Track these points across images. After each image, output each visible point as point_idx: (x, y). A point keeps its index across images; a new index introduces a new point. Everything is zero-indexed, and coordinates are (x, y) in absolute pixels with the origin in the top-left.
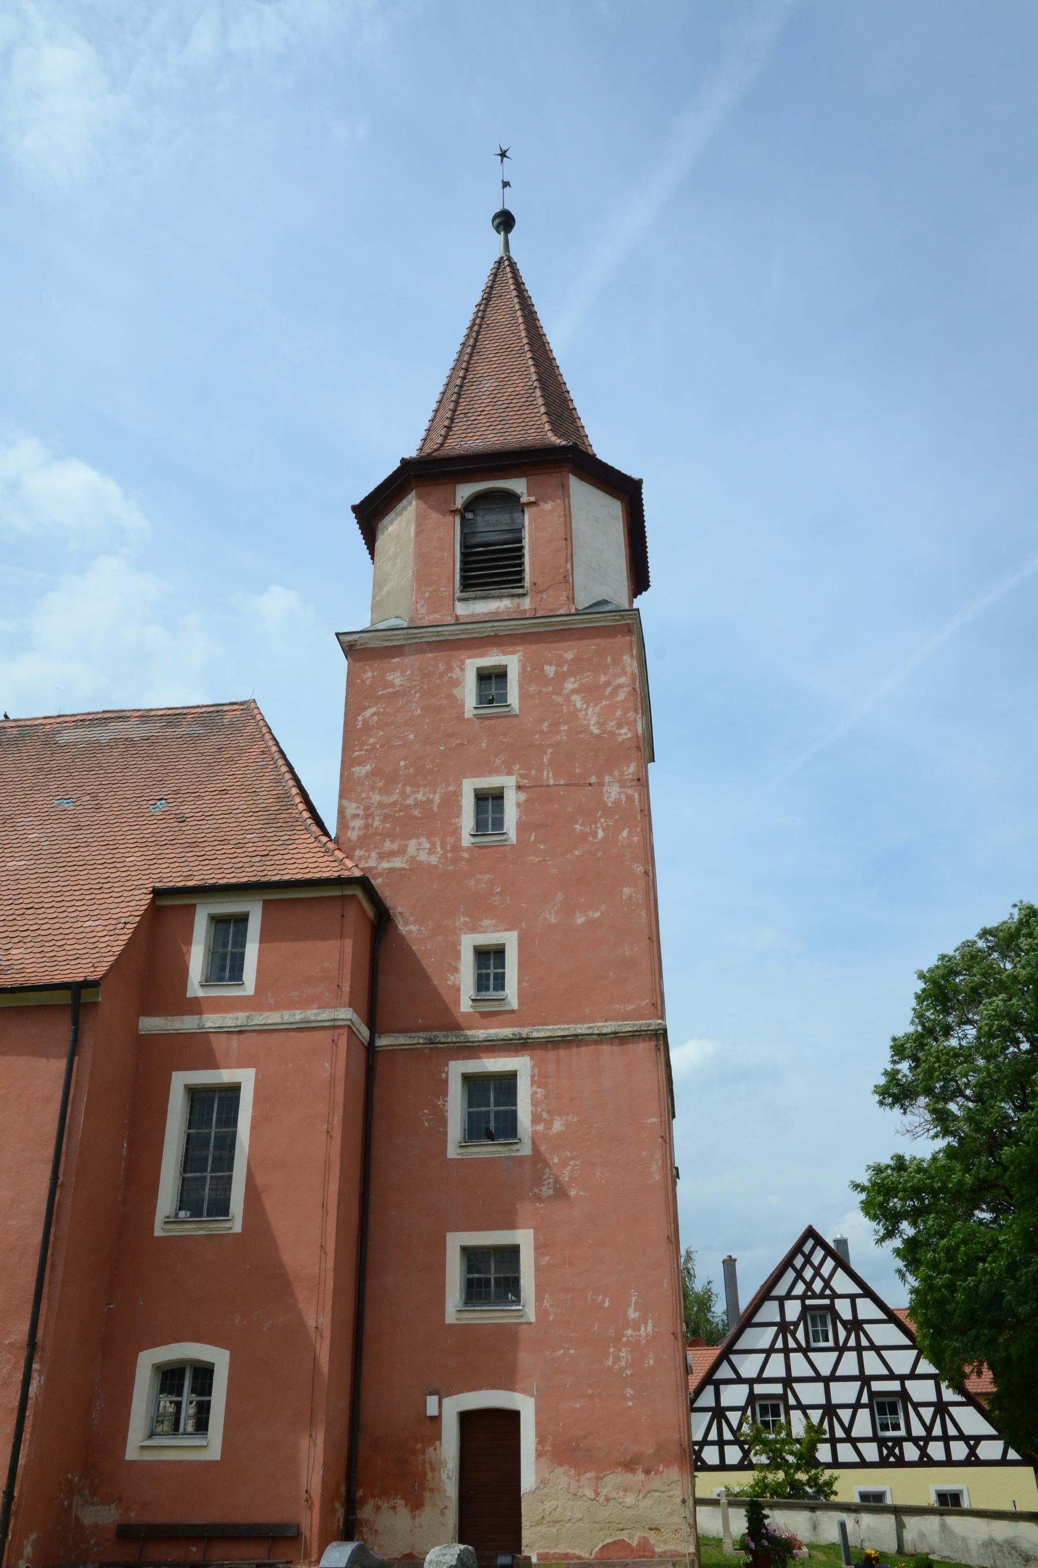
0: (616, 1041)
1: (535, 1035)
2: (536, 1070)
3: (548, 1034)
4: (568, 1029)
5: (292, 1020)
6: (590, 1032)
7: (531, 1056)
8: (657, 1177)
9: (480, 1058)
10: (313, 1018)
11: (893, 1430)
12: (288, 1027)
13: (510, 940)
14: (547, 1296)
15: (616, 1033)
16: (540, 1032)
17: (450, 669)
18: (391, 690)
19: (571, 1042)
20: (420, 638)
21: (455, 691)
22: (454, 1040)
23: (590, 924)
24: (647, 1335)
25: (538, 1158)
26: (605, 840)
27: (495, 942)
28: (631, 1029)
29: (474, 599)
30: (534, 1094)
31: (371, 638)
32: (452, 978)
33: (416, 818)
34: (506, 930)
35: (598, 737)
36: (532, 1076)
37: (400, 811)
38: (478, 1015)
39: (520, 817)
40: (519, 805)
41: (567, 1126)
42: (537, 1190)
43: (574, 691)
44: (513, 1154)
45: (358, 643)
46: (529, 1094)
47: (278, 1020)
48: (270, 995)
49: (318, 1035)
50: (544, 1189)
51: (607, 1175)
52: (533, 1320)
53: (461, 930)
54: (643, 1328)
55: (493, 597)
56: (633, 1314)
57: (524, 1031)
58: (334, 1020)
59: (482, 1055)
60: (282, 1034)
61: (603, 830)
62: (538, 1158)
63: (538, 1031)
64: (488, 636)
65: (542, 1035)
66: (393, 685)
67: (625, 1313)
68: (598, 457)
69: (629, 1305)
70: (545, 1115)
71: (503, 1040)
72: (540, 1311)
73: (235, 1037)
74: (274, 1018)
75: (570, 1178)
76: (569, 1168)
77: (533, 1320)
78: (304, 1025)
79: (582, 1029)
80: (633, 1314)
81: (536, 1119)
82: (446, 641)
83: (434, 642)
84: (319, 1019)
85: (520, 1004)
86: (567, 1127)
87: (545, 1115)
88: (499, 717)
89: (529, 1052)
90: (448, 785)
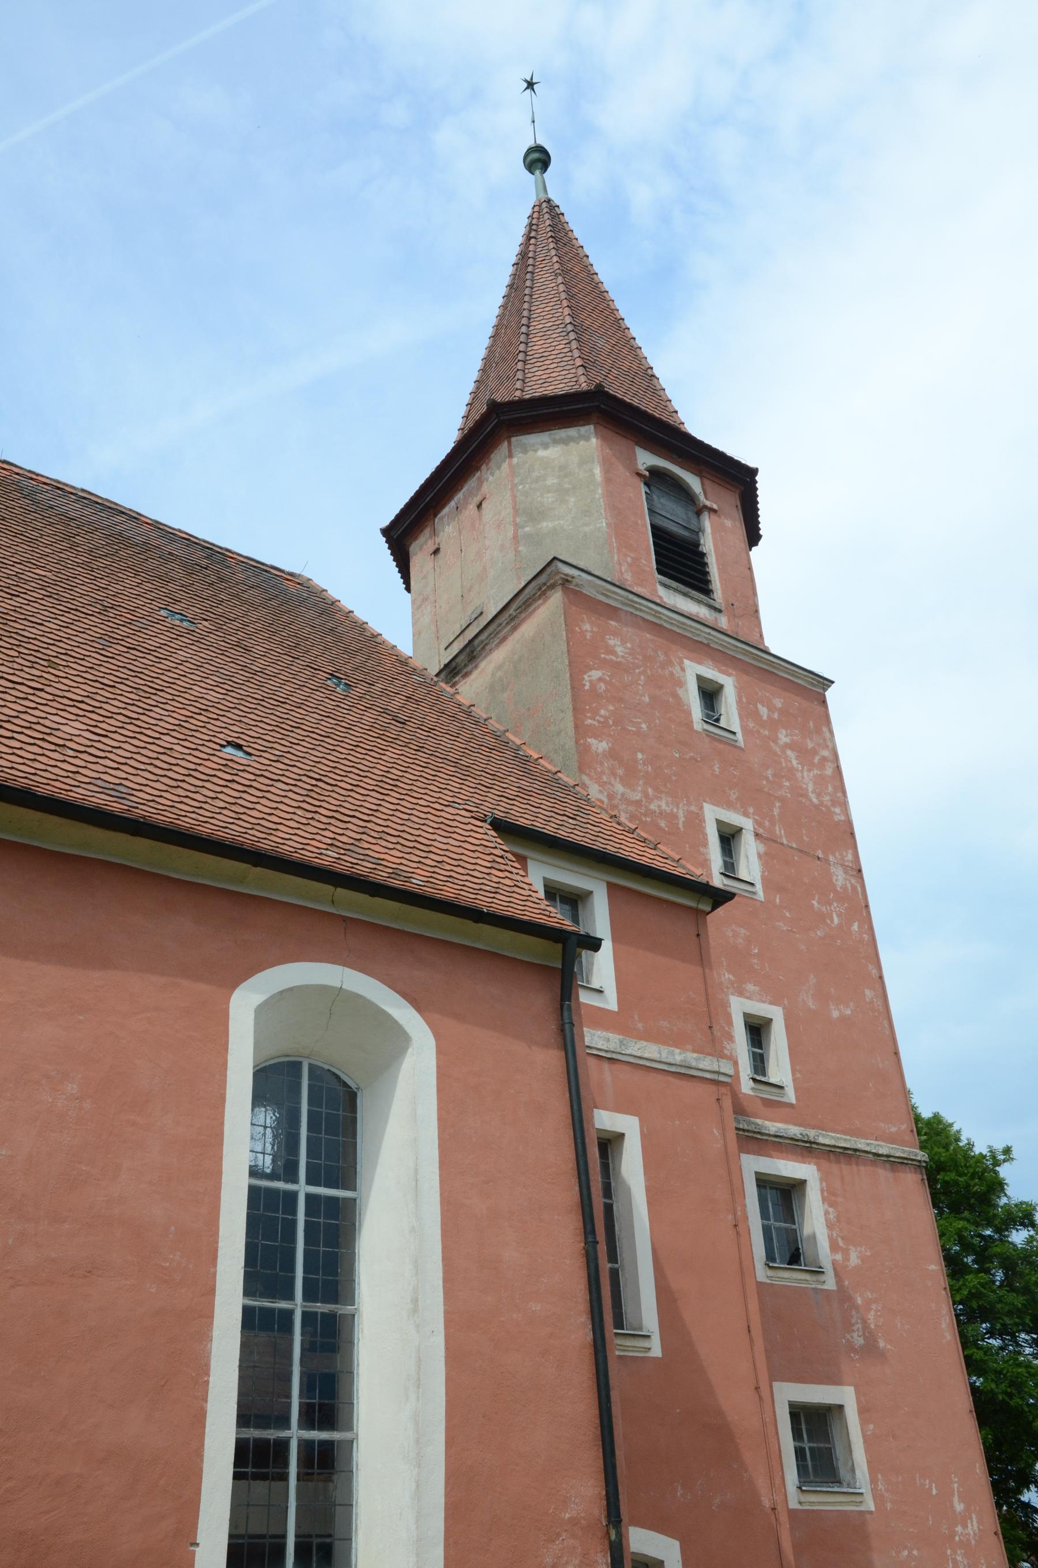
0: (888, 1166)
1: (821, 1140)
2: (824, 1184)
3: (832, 1142)
4: (850, 1140)
5: (670, 1060)
6: (868, 1149)
7: (816, 1164)
8: (949, 1338)
9: (771, 1156)
10: (694, 1064)
11: (243, 1452)
12: (666, 1067)
13: (775, 1014)
14: (880, 1476)
15: (888, 1156)
16: (826, 1139)
17: (670, 663)
18: (613, 657)
19: (850, 1156)
20: (637, 609)
21: (680, 692)
22: (746, 1127)
23: (843, 1018)
24: (975, 1534)
25: (843, 1295)
26: (840, 926)
27: (762, 1014)
28: (902, 1155)
29: (675, 590)
30: (826, 1213)
31: (589, 582)
32: (728, 1047)
33: (660, 829)
34: (771, 1003)
35: (817, 807)
36: (822, 1191)
37: (645, 815)
38: (759, 1102)
39: (763, 872)
40: (760, 856)
41: (863, 1259)
42: (848, 1336)
43: (787, 746)
44: (819, 1287)
45: (575, 581)
46: (823, 1213)
47: (655, 1056)
48: (636, 1017)
49: (699, 1089)
50: (855, 1335)
51: (907, 1327)
52: (873, 1509)
53: (727, 988)
54: (969, 1525)
55: (692, 598)
56: (959, 1507)
57: (812, 1134)
58: (718, 1073)
59: (773, 1153)
60: (660, 1077)
61: (838, 916)
62: (843, 1295)
63: (823, 1136)
64: (701, 642)
65: (827, 1141)
66: (614, 653)
67: (952, 1506)
68: (384, 539)
69: (953, 1495)
70: (841, 1243)
71: (792, 1139)
72: (877, 1497)
73: (606, 1065)
74: (650, 1050)
75: (876, 1325)
76: (872, 1313)
77: (873, 1509)
78: (683, 1071)
79: (861, 1144)
80: (959, 1507)
81: (834, 1247)
82: (661, 626)
83: (648, 621)
84: (701, 1066)
85: (797, 1098)
86: (862, 1261)
87: (841, 1243)
88: (726, 743)
89: (815, 1160)
90: (689, 804)
